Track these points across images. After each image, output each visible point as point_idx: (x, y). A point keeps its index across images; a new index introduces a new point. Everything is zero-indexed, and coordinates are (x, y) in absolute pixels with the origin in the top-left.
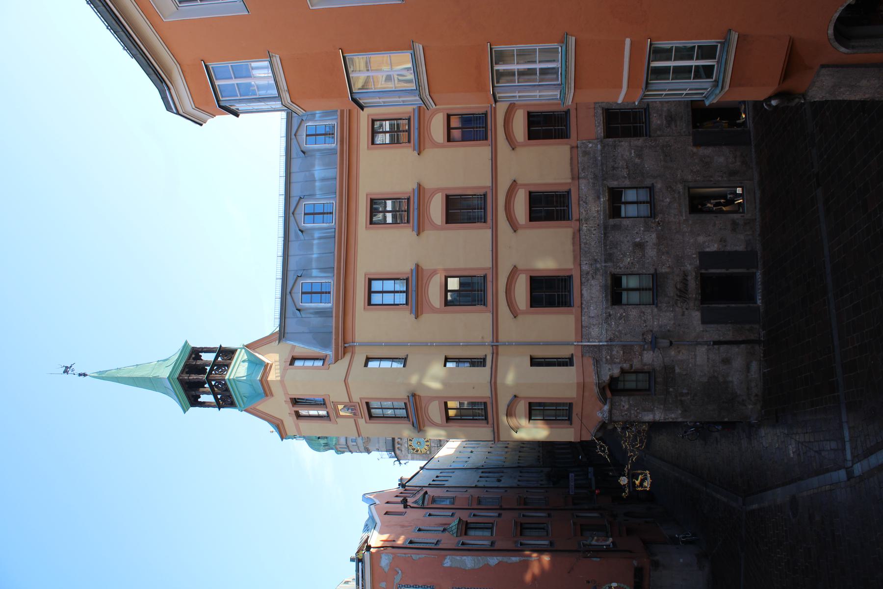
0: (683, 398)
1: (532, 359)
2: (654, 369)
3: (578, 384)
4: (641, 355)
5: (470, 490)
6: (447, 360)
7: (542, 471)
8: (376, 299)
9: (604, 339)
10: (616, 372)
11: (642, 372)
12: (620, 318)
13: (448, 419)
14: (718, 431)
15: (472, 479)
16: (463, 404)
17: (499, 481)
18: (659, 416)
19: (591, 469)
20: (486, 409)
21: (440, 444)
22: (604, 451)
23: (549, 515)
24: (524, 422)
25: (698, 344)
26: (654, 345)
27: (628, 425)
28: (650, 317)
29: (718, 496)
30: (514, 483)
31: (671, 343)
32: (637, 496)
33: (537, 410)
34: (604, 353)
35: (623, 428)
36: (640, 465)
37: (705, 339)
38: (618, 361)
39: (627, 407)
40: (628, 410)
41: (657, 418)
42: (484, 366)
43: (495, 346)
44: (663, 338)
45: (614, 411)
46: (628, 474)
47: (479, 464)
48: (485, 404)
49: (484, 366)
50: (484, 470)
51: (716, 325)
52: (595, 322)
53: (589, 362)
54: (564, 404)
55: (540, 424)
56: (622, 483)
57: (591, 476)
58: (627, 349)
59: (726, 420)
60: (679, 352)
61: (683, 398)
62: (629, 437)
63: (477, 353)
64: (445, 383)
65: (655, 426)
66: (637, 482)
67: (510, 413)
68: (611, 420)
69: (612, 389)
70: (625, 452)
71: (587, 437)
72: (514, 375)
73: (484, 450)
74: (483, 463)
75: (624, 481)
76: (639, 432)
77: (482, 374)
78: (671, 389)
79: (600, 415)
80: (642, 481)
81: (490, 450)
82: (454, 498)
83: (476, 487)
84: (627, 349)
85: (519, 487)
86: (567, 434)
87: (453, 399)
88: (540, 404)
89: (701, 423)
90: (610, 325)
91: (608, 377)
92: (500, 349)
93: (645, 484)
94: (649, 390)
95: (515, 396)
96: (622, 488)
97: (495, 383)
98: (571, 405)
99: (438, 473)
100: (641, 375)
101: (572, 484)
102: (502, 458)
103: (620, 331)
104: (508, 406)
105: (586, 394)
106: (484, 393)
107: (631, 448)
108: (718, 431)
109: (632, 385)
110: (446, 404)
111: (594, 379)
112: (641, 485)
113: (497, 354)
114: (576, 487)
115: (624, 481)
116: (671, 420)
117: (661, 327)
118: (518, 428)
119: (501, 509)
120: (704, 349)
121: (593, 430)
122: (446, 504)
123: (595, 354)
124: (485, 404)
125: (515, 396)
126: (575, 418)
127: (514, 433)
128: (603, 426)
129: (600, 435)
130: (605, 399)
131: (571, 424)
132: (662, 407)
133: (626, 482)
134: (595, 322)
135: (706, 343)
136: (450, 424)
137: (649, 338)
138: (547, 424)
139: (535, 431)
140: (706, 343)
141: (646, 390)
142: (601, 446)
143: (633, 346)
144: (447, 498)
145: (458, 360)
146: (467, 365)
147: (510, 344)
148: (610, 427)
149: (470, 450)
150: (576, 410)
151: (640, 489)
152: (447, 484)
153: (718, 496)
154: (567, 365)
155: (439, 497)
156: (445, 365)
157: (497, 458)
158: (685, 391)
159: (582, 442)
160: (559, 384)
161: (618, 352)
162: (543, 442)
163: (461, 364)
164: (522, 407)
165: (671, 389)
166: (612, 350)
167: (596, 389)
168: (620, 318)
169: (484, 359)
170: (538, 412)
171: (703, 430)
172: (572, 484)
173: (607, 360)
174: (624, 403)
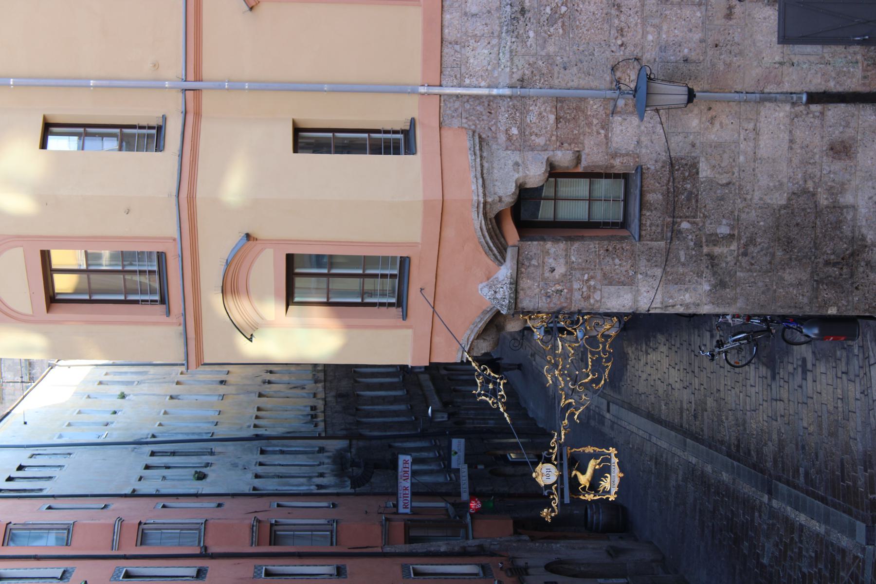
0: (717, 250)
1: (297, 131)
2: (640, 169)
3: (426, 203)
4: (605, 126)
5: (116, 505)
6: (48, 128)
7: (322, 450)
8: (190, 94)
9: (505, 80)
10: (535, 174)
11: (608, 176)
12: (551, 21)
13: (52, 299)
14: (809, 341)
15: (124, 472)
16: (99, 257)
17: (201, 477)
18: (646, 296)
19: (458, 444)
20: (162, 272)
21: (30, 373)
22: (494, 393)
23: (340, 572)
24: (272, 309)
25: (766, 98)
26: (643, 97)
27: (561, 323)
28: (634, 20)
29: (802, 518)
30: (244, 482)
31: (691, 96)
32: (577, 518)
33: (304, 275)
34: (503, 118)
35: (548, 331)
36: (592, 431)
37: (787, 88)
38: (541, 141)
39: (561, 270)
40: (566, 278)
41: (643, 305)
42: (159, 148)
43: (192, 93)
44: (671, 81)
45: (525, 283)
46: (560, 456)
47: (144, 433)
48: (161, 257)
49: (159, 148)
50: (158, 448)
51: (817, 48)
52: (479, 27)
53: (460, 144)
54: (385, 261)
55: (318, 315)
56: (542, 481)
57: (458, 461)
58: (567, 109)
59: (832, 311)
60: (712, 120)
61: (717, 250)
62: (565, 355)
63: (139, 110)
64: (45, 197)
65: (639, 327)
66: (584, 479)
67: (230, 287)
68: (516, 310)
69: (524, 217)
70: (550, 398)
71: (449, 353)
72: (248, 178)
73: (158, 389)
74: (154, 428)
75: (546, 474)
76: (592, 341)
77: (155, 169)
78: (685, 225)
79: (485, 293)
80: (598, 475)
81: (175, 389)
82: (69, 529)
83: (134, 495)
84: (567, 109)
85: (256, 494)
86: (391, 344)
87: (68, 242)
88: (319, 260)
89: (764, 319)
90: (522, 39)
91: (512, 188)
92: (207, 100)
93: (606, 484)
94: (624, 225)
95: (248, 236)
96: (541, 496)
97: (191, 199)
98: (404, 263)
99: (23, 457)
100: (604, 182)
101: (405, 484)
102: (212, 414)
103: (549, 59)
104: (228, 264)
105: (450, 233)
106: (156, 227)
107: (563, 374)
108: (809, 341)
109: (576, 211)
110: (45, 256)
111: (472, 191)
112: (594, 486)
113: (198, 114)
114: (417, 493)
115: (546, 474)
116: (681, 310)
117: (663, 49)
118: (255, 327)
119: (205, 554)
120: (781, 113)
121: (467, 332)
122: (48, 544)
123: (480, 123)
124: (161, 257)
125: (248, 236)
126: (414, 297)
127: (242, 341)
128: (494, 323)
129: (484, 347)
130: (502, 250)
131: (405, 316)
132: (658, 272)
133: (553, 478)
134: (479, 27)
135: (790, 97)
136: (54, 316)
137: (630, 78)
138: (339, 316)
139: (311, 337)
140: (790, 97)
141: (614, 225)
142: (487, 380)
143: (583, 99)
144: (49, 528)
145: (85, 130)
146: (112, 144)
147: (235, 86)
148: (513, 327)
149: (118, 389)
150: (420, 278)
151: (589, 497)
152: (49, 488)
153: (802, 518)
154: (397, 152)
155: (26, 527)
156: (44, 145)
157: (196, 410)
158: (724, 230)
159: (433, 368)
160: (372, 205)
161: (541, 118)
162: (326, 366)
163: (89, 142)
164: (268, 269)
165: (685, 225)
166: (525, 112)
167: (477, 221)
168: (551, 21)
169: (160, 129)
170: (312, 282)
171: (767, 338)
172: (405, 484)
173: (509, 138)
174: (554, 258)
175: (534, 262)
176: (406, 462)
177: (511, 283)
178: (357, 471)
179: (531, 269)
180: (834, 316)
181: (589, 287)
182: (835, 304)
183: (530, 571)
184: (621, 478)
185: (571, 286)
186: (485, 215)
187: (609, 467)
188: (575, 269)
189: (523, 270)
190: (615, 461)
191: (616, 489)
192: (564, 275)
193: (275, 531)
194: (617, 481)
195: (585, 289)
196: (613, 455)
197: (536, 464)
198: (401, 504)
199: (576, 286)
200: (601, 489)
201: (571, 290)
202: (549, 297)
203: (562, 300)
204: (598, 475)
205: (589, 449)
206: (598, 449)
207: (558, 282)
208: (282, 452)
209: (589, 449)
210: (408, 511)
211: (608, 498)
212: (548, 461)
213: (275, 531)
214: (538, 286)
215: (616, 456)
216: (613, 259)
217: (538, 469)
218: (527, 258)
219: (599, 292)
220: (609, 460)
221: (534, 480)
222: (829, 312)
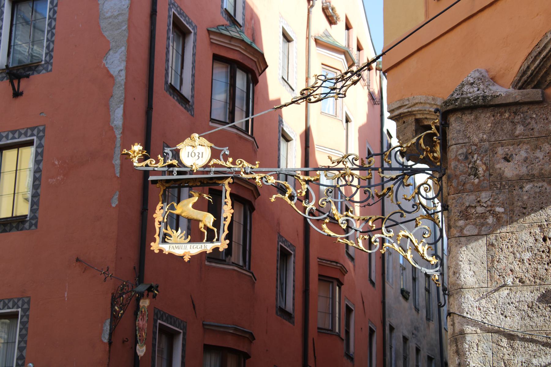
45: (486, 121)
112: (175, 221)
151: (159, 215)
175: (520, 129)
177: (484, 97)
179: (508, 126)
181: (483, 216)
184: (182, 258)
185: (484, 189)
188: (511, 192)
189: (507, 115)
190: (209, 247)
192: (501, 176)
193: (332, 282)
194: (178, 252)
195: (480, 210)
196: (216, 244)
197: (209, 138)
199: (484, 196)
200: (169, 231)
201: (478, 189)
202: (466, 158)
203: (462, 178)
204: (194, 233)
207: (489, 168)
209: (227, 211)
211: (154, 240)
212: (215, 154)
213: (332, 282)
214: (482, 140)
215: (216, 249)
217: (204, 141)
218: (525, 118)
219: (476, 232)
220: (210, 239)
221: (188, 135)
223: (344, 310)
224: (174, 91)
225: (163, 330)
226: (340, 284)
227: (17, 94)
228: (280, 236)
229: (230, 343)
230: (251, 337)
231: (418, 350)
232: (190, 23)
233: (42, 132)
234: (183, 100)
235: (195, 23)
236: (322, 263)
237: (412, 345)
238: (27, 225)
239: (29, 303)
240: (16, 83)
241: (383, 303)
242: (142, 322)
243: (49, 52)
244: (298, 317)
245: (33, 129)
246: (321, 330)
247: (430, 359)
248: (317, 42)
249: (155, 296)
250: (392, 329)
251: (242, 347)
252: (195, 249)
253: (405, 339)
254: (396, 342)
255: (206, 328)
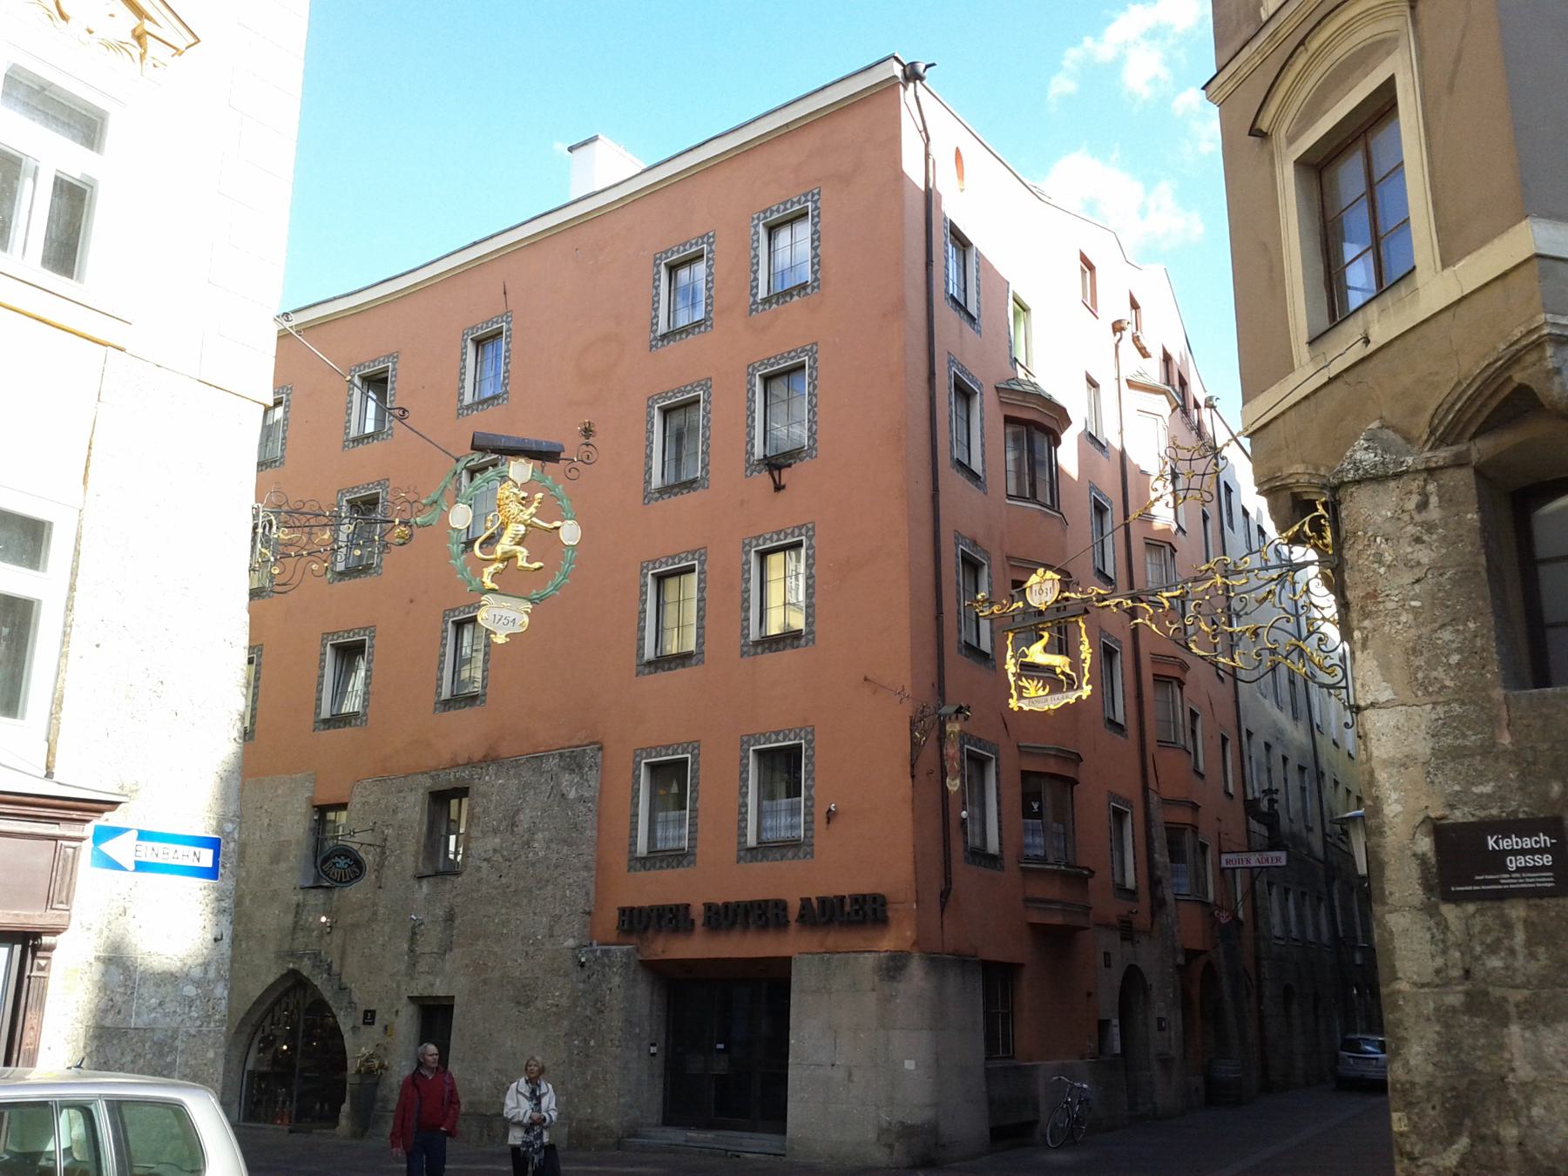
66: (1036, 653)
93: (1033, 688)
112: (1029, 669)
151: (1011, 667)
176: (1278, 859)
178: (1264, 806)
180: (1390, 1128)
182: (1414, 1127)
183: (1127, 945)
186: (1515, 360)
187: (1061, 691)
190: (1071, 698)
191: (1026, 708)
198: (1229, 856)
205: (1086, 651)
206: (1087, 666)
208: (1303, 789)
209: (1086, 651)
210: (1224, 864)
216: (1459, 650)
220: (1071, 687)
222: (1395, 1116)
223: (1187, 714)
224: (964, 467)
225: (972, 756)
226: (1181, 684)
227: (779, 488)
228: (1102, 630)
229: (1052, 767)
230: (1077, 759)
231: (1285, 759)
232: (974, 382)
233: (811, 531)
234: (973, 476)
235: (980, 380)
236: (1157, 659)
237: (1278, 752)
238: (803, 641)
239: (812, 732)
240: (776, 473)
241: (1237, 702)
242: (952, 750)
243: (812, 435)
244: (1132, 728)
245: (800, 528)
246: (1161, 743)
247: (1302, 769)
248: (1131, 384)
249: (967, 718)
250: (1249, 734)
251: (1067, 771)
252: (1055, 702)
253: (1268, 746)
254: (1257, 750)
255: (1023, 751)
